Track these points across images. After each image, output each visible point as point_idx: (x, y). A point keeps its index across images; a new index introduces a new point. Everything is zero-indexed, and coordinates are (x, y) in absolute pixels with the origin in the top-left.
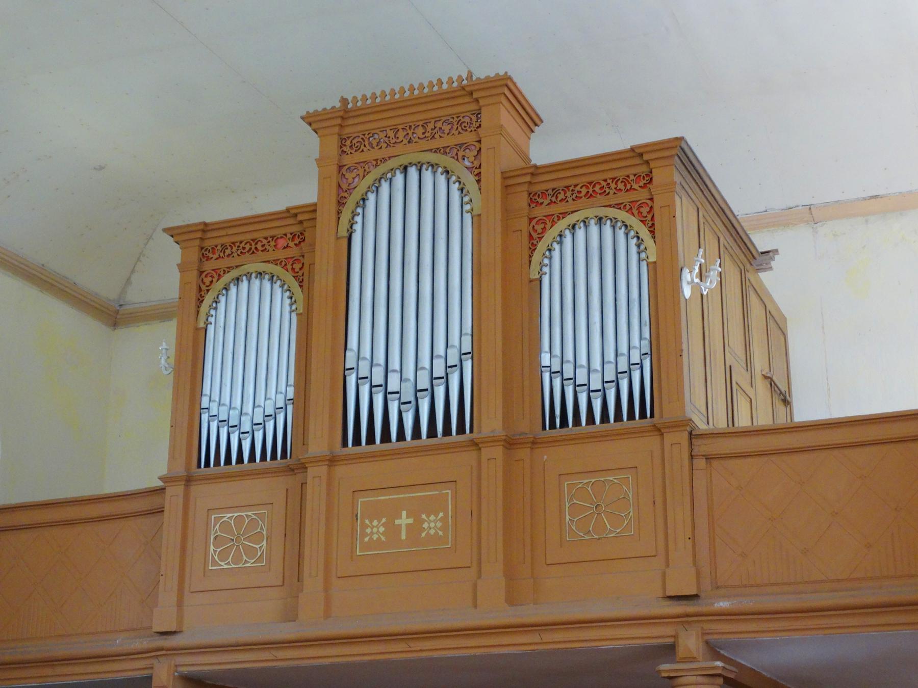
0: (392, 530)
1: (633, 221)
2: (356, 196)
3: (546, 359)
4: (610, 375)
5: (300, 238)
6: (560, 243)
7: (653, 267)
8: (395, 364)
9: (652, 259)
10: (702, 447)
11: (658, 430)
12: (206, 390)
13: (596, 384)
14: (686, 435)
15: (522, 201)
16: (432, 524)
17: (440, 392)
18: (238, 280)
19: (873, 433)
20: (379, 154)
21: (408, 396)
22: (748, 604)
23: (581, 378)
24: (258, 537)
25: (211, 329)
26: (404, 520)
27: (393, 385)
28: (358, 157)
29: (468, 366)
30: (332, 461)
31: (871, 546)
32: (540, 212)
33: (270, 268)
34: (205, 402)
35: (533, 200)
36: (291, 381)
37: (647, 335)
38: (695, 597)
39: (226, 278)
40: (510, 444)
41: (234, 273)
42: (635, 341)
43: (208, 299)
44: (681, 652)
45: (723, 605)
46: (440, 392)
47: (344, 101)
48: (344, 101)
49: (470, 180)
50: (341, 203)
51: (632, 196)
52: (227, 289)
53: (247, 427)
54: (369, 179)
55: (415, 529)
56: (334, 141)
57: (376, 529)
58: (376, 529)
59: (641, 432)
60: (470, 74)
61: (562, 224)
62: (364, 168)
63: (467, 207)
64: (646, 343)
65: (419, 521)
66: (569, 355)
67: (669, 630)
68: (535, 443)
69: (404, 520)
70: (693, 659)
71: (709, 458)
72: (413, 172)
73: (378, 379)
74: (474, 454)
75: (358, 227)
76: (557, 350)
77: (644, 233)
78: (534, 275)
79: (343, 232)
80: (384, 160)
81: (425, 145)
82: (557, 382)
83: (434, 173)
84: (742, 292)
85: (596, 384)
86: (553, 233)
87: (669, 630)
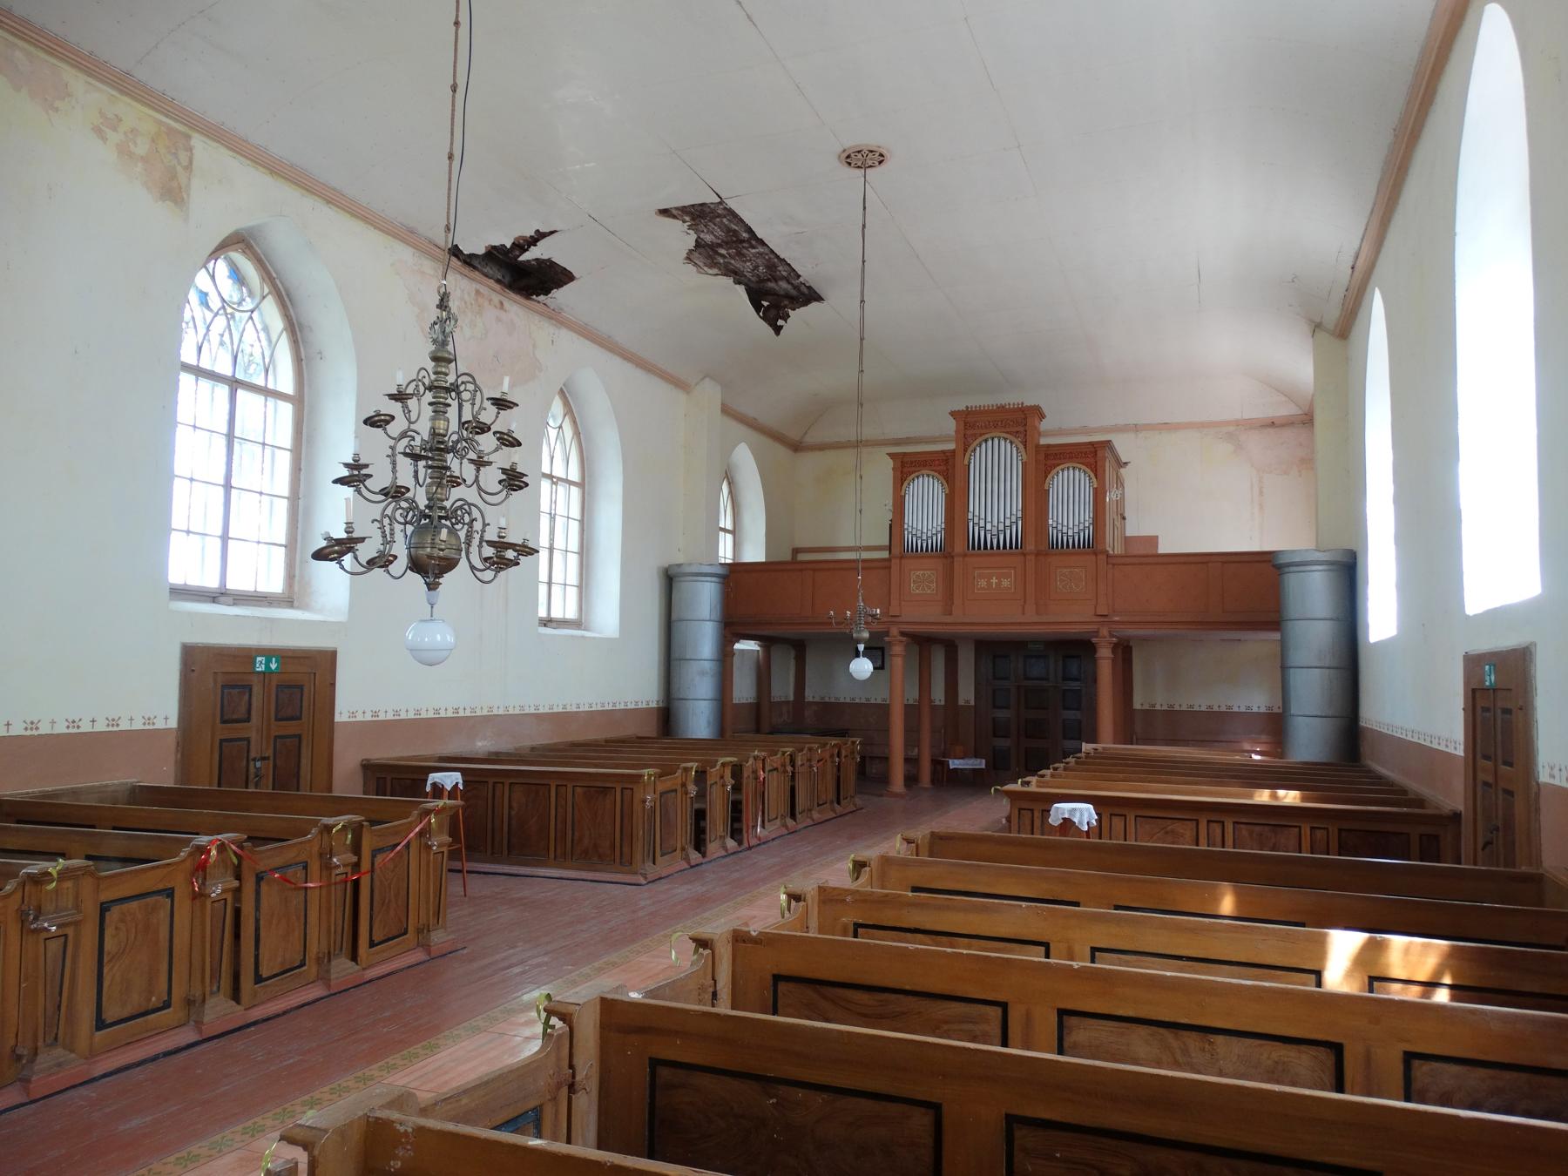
0: (990, 584)
1: (1088, 470)
2: (971, 448)
3: (1050, 522)
4: (1076, 530)
5: (946, 462)
6: (980, 446)
7: (1096, 490)
8: (989, 519)
9: (1095, 486)
10: (1110, 560)
11: (1095, 554)
12: (906, 521)
13: (1070, 533)
14: (1105, 557)
15: (1042, 457)
16: (1005, 583)
17: (1008, 532)
18: (918, 477)
19: (1182, 559)
20: (982, 432)
21: (995, 532)
22: (1125, 619)
23: (1065, 530)
24: (932, 582)
25: (907, 496)
26: (994, 580)
27: (989, 527)
28: (971, 432)
29: (1020, 523)
30: (965, 555)
31: (550, 1012)
32: (1049, 462)
33: (933, 473)
34: (906, 526)
35: (1047, 456)
36: (943, 521)
37: (1091, 516)
38: (1107, 616)
39: (913, 476)
40: (1038, 554)
41: (917, 474)
42: (1087, 518)
43: (905, 484)
44: (1101, 634)
45: (1117, 619)
46: (1008, 532)
47: (967, 407)
48: (967, 407)
49: (1021, 447)
50: (965, 451)
51: (1088, 460)
52: (913, 480)
53: (924, 538)
54: (977, 441)
55: (999, 584)
56: (962, 424)
57: (983, 583)
58: (983, 583)
59: (1088, 554)
60: (1022, 403)
61: (1058, 468)
62: (975, 437)
63: (1020, 458)
64: (1091, 520)
65: (1000, 582)
66: (1060, 521)
67: (1096, 627)
68: (1046, 554)
69: (994, 580)
70: (1105, 637)
71: (1114, 565)
72: (996, 440)
73: (982, 524)
74: (1094, 557)
75: (972, 461)
76: (1055, 519)
77: (1092, 475)
78: (1046, 488)
79: (966, 463)
80: (984, 434)
81: (1003, 430)
82: (1055, 531)
83: (1005, 442)
84: (449, 204)
85: (1070, 533)
86: (1055, 471)
87: (1096, 627)
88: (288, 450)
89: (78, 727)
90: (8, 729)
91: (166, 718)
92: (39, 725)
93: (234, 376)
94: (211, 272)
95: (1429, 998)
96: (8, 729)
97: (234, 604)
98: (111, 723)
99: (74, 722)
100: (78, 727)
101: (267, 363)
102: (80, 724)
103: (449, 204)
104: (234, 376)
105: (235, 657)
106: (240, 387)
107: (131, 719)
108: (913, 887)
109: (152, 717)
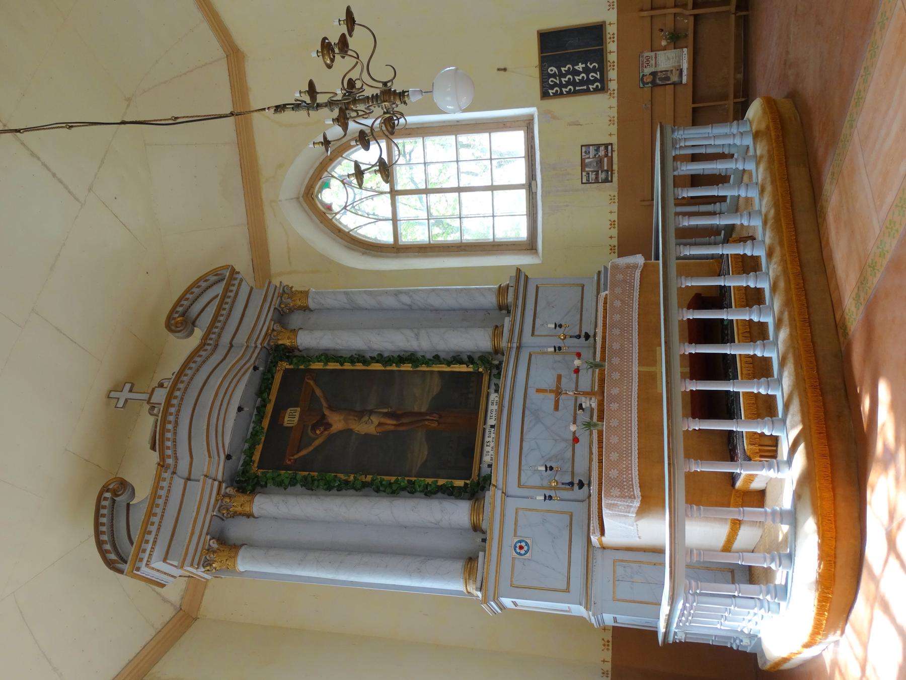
84: (78, 126)
88: (318, 93)
89: (613, 34)
90: (607, 629)
91: (611, 212)
92: (612, 220)
93: (389, 193)
94: (376, 220)
95: (106, 541)
96: (607, 629)
97: (535, 180)
98: (612, 122)
99: (610, 6)
100: (614, 62)
101: (377, 193)
102: (606, 640)
103: (78, 126)
104: (389, 193)
105: (542, 61)
106: (394, 189)
107: (611, 212)
108: (537, 389)
109: (609, 4)
